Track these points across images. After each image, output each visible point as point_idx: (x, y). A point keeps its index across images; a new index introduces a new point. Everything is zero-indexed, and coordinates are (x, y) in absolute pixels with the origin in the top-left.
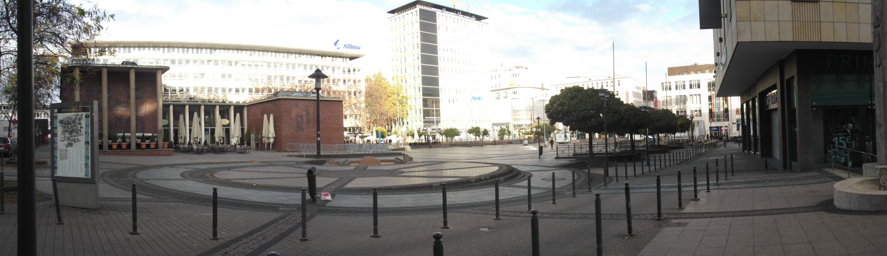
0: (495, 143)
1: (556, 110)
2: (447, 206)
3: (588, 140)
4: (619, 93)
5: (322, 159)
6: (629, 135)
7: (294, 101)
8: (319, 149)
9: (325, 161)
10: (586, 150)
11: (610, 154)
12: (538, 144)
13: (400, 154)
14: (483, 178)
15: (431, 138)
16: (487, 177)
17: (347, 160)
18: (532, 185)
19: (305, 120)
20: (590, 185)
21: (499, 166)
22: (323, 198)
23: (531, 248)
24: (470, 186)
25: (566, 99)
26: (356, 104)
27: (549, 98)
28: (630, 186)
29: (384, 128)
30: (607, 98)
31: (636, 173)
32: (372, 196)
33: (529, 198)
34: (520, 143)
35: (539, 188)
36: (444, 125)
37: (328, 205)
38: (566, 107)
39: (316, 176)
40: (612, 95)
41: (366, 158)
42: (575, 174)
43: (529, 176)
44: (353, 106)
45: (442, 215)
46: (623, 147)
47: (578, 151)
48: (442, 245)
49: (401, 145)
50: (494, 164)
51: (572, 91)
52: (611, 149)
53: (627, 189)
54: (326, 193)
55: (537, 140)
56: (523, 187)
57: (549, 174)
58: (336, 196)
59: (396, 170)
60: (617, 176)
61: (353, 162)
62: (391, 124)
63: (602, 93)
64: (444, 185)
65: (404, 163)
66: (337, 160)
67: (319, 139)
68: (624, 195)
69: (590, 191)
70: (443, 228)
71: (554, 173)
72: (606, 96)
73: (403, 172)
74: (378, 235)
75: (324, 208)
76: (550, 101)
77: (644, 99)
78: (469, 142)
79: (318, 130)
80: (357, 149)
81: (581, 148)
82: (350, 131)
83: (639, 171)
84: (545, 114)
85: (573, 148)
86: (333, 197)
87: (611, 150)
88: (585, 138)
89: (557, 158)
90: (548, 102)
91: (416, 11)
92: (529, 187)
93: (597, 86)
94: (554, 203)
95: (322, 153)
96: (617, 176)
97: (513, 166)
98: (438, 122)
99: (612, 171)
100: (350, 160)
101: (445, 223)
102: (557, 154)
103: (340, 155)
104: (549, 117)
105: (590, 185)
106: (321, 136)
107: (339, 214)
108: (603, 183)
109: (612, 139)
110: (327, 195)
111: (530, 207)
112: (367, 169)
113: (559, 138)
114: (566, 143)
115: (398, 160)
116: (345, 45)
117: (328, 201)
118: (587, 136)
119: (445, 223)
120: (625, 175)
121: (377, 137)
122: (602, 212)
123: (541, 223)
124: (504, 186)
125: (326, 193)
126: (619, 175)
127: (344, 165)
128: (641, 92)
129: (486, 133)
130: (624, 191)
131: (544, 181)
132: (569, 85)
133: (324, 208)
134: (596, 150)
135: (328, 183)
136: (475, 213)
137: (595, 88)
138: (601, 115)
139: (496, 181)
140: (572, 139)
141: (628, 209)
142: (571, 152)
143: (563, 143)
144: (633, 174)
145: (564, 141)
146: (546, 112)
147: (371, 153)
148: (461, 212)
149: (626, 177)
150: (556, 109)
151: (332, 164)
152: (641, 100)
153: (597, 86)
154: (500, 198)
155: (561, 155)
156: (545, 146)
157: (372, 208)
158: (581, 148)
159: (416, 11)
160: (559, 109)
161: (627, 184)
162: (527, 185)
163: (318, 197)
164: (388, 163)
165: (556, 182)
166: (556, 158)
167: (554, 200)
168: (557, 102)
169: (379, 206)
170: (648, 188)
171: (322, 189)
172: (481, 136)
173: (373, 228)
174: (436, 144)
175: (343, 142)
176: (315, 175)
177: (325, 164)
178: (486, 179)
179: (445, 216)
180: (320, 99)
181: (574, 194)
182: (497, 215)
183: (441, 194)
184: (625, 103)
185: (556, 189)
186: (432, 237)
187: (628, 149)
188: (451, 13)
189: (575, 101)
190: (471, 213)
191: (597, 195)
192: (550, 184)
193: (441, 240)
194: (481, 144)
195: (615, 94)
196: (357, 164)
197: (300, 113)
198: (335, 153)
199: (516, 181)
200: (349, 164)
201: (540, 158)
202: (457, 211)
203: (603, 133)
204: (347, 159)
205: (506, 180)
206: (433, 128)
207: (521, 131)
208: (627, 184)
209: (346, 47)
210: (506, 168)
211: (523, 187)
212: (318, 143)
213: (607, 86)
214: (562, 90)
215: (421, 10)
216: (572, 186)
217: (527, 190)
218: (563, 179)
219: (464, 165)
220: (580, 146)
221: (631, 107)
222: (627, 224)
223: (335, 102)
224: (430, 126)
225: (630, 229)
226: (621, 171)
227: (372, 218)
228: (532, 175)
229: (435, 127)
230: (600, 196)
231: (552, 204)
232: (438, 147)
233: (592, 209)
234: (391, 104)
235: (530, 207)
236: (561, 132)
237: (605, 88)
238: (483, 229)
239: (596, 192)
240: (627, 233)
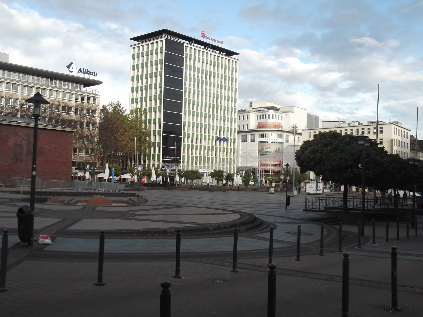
0: (238, 189)
1: (307, 158)
2: (181, 254)
3: (343, 193)
4: (383, 141)
5: (44, 196)
6: (393, 190)
7: (13, 127)
8: (33, 184)
9: (46, 198)
10: (339, 203)
11: (368, 210)
12: (285, 193)
13: (134, 195)
14: (222, 226)
15: (169, 180)
16: (227, 226)
17: (73, 199)
18: (275, 237)
19: (25, 151)
20: (340, 244)
21: (240, 214)
22: (41, 241)
23: (267, 307)
24: (208, 234)
25: (319, 145)
26: (89, 136)
27: (300, 144)
28: (398, 251)
29: (117, 165)
30: (367, 146)
31: (400, 236)
32: (99, 240)
33: (271, 252)
34: (266, 191)
35: (282, 242)
36: (184, 166)
37: (46, 249)
38: (319, 155)
39: (35, 216)
40: (373, 143)
41: (96, 197)
42: (325, 230)
43: (271, 228)
44: (84, 138)
45: (174, 263)
46: (384, 204)
47: (331, 204)
48: (170, 295)
49: (136, 185)
50: (235, 212)
51: (328, 136)
52: (369, 205)
53: (394, 255)
54: (45, 236)
55: (285, 189)
56: (265, 239)
57: (294, 228)
58: (58, 239)
59: (128, 212)
60: (374, 237)
61: (80, 201)
62: (127, 161)
63: (361, 140)
64: (178, 231)
65: (138, 205)
66: (61, 198)
67: (34, 173)
68: (390, 261)
69: (340, 250)
70: (174, 277)
71: (299, 226)
72: (366, 144)
73: (136, 215)
74: (103, 283)
75: (42, 253)
76: (301, 147)
77: (412, 149)
78: (211, 186)
79: (34, 162)
80: (86, 187)
81: (334, 201)
82: (79, 166)
83: (403, 233)
84: (295, 161)
85: (325, 201)
86: (52, 241)
87: (369, 206)
88: (340, 190)
89: (306, 210)
90: (299, 148)
91: (162, 41)
92: (271, 240)
93: (358, 132)
94: (298, 259)
95: (38, 189)
96: (374, 237)
97: (257, 216)
98: (178, 162)
99: (368, 231)
100: (76, 199)
101: (177, 272)
102: (306, 205)
103: (65, 192)
104: (299, 164)
105: (340, 244)
106: (37, 169)
107: (59, 260)
108: (357, 244)
109: (372, 193)
110: (46, 238)
111: (270, 261)
112: (96, 209)
113: (311, 188)
114: (318, 194)
115: (131, 202)
116: (80, 69)
117: (47, 245)
118: (342, 188)
119: (177, 272)
120: (386, 237)
121: (110, 175)
122: (351, 275)
123: (279, 279)
124: (244, 236)
125: (45, 236)
126: (376, 235)
127: (70, 204)
128: (408, 141)
129: (230, 177)
130: (390, 256)
131: (288, 234)
132: (325, 130)
133: (42, 253)
134: (351, 205)
135: (55, 222)
136: (211, 263)
137: (355, 134)
138: (359, 165)
139: (236, 230)
140: (325, 190)
141: (394, 278)
142: (323, 205)
143: (314, 194)
144: (395, 236)
145: (315, 192)
146: (296, 159)
147: (102, 191)
148: (195, 261)
149: (387, 239)
150: (307, 156)
151: (55, 202)
152: (408, 151)
153: (358, 132)
154: (239, 249)
155: (310, 207)
156: (293, 196)
157: (97, 253)
158: (334, 201)
159: (162, 41)
160: (311, 157)
161: (394, 249)
162: (269, 237)
163: (35, 241)
164: (120, 205)
165: (302, 237)
166: (304, 210)
167: (298, 256)
168: (310, 149)
169: (105, 251)
170: (415, 255)
171: (40, 231)
172: (224, 181)
173: (97, 276)
174: (174, 186)
175: (71, 178)
176: (33, 214)
177: (47, 203)
178: (225, 227)
179: (178, 265)
180: (38, 127)
181: (322, 252)
182: (234, 267)
183: (175, 241)
184: (389, 153)
185: (301, 245)
186: (160, 286)
187: (390, 207)
188: (199, 46)
189: (329, 148)
190: (206, 263)
191: (346, 256)
192: (294, 239)
193: (169, 289)
194: (224, 189)
195: (379, 141)
196: (85, 204)
197: (19, 142)
198: (60, 190)
199: (258, 232)
200: (75, 204)
201: (286, 208)
202: (192, 260)
203: (361, 186)
204: (72, 198)
205: (247, 230)
206: (172, 168)
207: (268, 177)
208: (394, 249)
209: (81, 71)
210: (248, 217)
211: (265, 239)
212: (34, 178)
213: (369, 133)
214: (315, 136)
215: (166, 40)
216: (320, 243)
217: (268, 243)
218: (311, 234)
219: (203, 211)
220: (333, 199)
221: (396, 158)
222: (391, 296)
223: (63, 133)
224: (169, 166)
225: (394, 302)
226: (381, 231)
227: (97, 264)
228: (276, 227)
229: (175, 167)
230: (349, 257)
231: (296, 260)
232: (176, 190)
233: (339, 271)
234: (127, 139)
235: (270, 261)
236: (312, 181)
237: (366, 135)
238: (219, 281)
239: (345, 252)
240: (390, 305)
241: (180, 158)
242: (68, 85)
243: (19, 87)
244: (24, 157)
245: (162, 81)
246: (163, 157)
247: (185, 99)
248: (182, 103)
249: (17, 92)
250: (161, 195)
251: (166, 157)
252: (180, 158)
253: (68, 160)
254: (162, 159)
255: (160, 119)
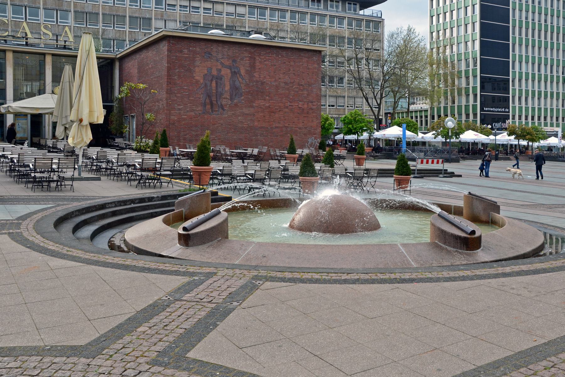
19: (227, 88)
197: (215, 72)
241: (508, 110)
242: (337, 7)
243: (268, 12)
244: (225, 100)
245: (476, 66)
246: (482, 109)
247: (514, 38)
248: (509, 44)
249: (265, 19)
250: (508, 190)
251: (486, 109)
252: (508, 110)
253: (313, 105)
254: (480, 112)
255: (474, 88)
